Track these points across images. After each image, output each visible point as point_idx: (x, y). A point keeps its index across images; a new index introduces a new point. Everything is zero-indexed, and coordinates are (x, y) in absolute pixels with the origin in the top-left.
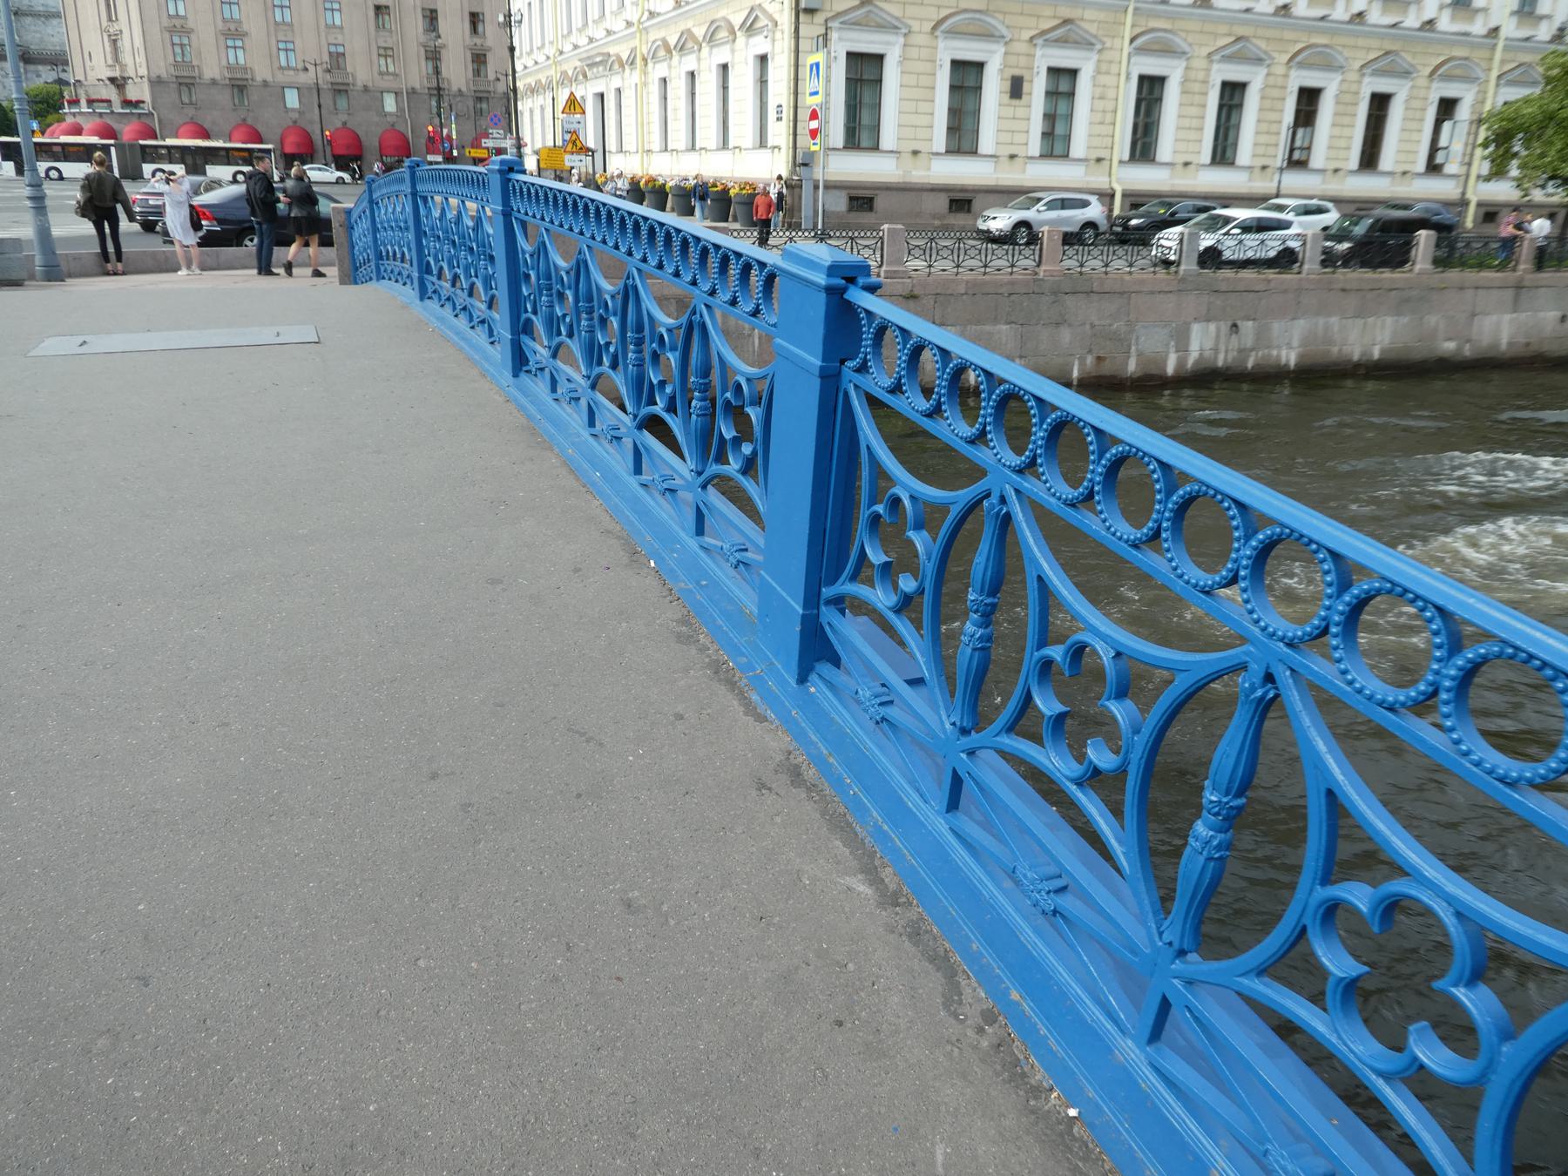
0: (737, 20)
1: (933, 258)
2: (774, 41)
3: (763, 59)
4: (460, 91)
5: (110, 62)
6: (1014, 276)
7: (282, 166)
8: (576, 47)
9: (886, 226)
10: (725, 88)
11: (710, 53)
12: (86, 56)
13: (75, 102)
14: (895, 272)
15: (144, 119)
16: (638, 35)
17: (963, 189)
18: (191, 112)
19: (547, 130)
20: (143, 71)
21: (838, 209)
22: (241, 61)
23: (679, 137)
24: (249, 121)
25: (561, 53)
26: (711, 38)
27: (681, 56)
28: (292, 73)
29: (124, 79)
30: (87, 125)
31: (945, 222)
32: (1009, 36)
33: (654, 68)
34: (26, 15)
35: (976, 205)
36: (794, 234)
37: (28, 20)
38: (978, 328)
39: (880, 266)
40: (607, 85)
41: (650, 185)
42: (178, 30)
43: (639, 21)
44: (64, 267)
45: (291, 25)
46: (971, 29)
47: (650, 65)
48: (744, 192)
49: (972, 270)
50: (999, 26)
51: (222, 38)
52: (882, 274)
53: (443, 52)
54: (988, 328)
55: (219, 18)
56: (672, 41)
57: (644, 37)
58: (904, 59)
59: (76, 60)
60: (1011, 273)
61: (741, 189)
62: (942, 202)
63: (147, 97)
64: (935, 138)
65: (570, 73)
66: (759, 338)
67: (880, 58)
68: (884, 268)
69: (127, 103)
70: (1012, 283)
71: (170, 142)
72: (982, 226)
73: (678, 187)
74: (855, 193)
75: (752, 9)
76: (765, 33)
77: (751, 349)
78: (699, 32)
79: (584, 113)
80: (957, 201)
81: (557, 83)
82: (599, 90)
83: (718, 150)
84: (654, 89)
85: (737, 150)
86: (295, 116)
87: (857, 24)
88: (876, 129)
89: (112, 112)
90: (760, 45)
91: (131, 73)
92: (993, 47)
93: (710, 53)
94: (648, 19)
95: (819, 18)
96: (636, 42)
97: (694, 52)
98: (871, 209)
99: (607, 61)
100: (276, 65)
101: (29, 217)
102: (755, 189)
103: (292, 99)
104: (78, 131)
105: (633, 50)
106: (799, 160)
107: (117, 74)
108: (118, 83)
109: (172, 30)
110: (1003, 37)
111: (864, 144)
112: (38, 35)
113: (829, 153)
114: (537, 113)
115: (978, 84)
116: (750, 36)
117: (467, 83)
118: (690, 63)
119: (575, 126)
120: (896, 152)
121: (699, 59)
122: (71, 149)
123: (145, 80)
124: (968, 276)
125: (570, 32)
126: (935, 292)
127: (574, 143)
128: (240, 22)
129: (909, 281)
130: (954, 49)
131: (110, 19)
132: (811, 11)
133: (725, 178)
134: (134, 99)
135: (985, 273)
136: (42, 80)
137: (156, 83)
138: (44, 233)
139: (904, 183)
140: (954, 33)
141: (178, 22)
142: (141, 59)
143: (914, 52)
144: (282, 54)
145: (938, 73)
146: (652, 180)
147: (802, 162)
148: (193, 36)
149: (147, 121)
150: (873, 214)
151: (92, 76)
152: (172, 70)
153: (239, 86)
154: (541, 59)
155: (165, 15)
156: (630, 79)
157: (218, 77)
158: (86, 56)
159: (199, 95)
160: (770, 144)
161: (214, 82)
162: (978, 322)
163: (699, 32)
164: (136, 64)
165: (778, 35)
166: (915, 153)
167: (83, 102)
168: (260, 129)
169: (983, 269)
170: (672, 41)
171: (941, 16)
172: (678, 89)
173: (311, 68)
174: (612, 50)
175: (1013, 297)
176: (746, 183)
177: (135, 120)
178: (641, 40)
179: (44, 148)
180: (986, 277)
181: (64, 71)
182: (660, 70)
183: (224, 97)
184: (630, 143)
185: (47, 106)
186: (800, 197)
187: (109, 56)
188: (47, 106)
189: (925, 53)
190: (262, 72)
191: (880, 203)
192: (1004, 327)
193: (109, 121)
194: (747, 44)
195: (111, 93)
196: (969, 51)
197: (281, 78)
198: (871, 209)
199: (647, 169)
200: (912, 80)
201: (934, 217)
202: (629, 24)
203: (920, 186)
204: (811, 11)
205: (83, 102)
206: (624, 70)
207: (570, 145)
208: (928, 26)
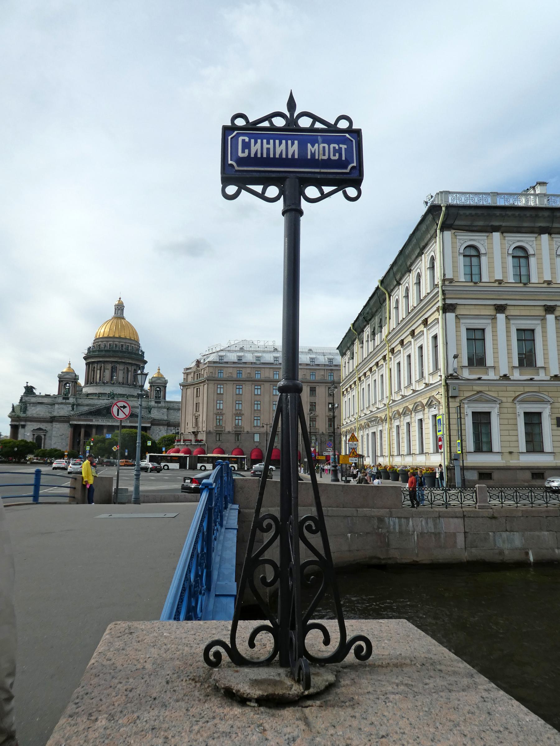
0: (425, 402)
1: (518, 500)
2: (439, 409)
3: (421, 421)
4: (323, 433)
5: (194, 426)
6: (549, 508)
7: (249, 464)
8: (366, 414)
9: (477, 486)
10: (421, 428)
11: (415, 415)
12: (186, 424)
13: (179, 441)
14: (483, 506)
15: (202, 447)
16: (388, 409)
17: (538, 468)
18: (219, 444)
19: (364, 446)
20: (204, 429)
21: (474, 479)
22: (240, 424)
23: (416, 448)
24: (240, 447)
25: (360, 417)
26: (415, 410)
27: (404, 417)
28: (258, 428)
29: (198, 432)
30: (181, 449)
31: (530, 484)
32: (552, 401)
33: (394, 422)
34: (171, 409)
35: (546, 475)
36: (432, 489)
37: (172, 411)
38: (531, 533)
39: (476, 504)
40: (377, 429)
41: (391, 470)
42: (219, 414)
43: (388, 404)
44: (142, 499)
45: (260, 410)
46: (532, 399)
47: (393, 421)
48: (428, 472)
49: (525, 505)
50: (546, 397)
51: (234, 416)
52: (477, 507)
53: (317, 418)
54: (537, 533)
55: (234, 409)
56: (401, 411)
57: (390, 410)
58: (500, 414)
59: (183, 425)
60: (547, 507)
61: (427, 471)
62: (528, 475)
63: (204, 439)
64: (520, 446)
65: (363, 425)
66: (417, 536)
67: (489, 413)
68: (478, 504)
69: (197, 441)
70: (547, 511)
71: (209, 455)
72: (547, 485)
73: (402, 470)
74: (481, 471)
75: (430, 398)
76: (434, 407)
77: (413, 541)
78: (411, 407)
79: (358, 441)
80: (535, 474)
81: (358, 428)
82: (373, 431)
83: (419, 454)
84: (395, 430)
85: (427, 454)
86: (257, 444)
87: (476, 401)
88: (490, 443)
89: (191, 444)
90: (434, 411)
91: (200, 430)
92: (545, 406)
93: (415, 415)
94: (392, 403)
95: (458, 400)
96: (387, 412)
97: (409, 415)
98: (491, 478)
99: (376, 419)
100: (253, 426)
101: (133, 482)
102: (433, 471)
103: (257, 438)
104: (178, 451)
105: (386, 415)
106: (453, 458)
107: (195, 430)
108: (195, 434)
109: (217, 414)
110: (549, 401)
111: (485, 449)
112: (174, 416)
113: (467, 454)
114: (365, 437)
115: (540, 422)
116: (430, 408)
117: (326, 430)
118: (408, 419)
119: (354, 446)
120: (501, 453)
121: (411, 418)
122: (174, 458)
123: (205, 432)
124: (524, 508)
125: (364, 409)
126: (506, 516)
127: (353, 453)
128: (241, 410)
129: (491, 510)
130: (525, 408)
131: (196, 411)
132: (454, 397)
133: (421, 466)
134: (200, 439)
135: (532, 507)
136: (172, 432)
137: (208, 433)
138: (137, 487)
139: (506, 466)
140: (523, 401)
141: (219, 411)
142: (205, 425)
143: (505, 410)
144: (255, 421)
145: (518, 418)
146: (392, 467)
147: (454, 458)
148: (224, 416)
149: (202, 447)
150: (492, 481)
151: (187, 431)
152: (215, 429)
153: (238, 434)
154: (353, 420)
155: (216, 409)
156: (386, 426)
157: (231, 430)
158: (186, 424)
159: (223, 437)
160: (425, 452)
161: (229, 432)
162: (531, 530)
163: (411, 407)
164: (203, 427)
165: (441, 407)
166: (511, 453)
167: (182, 441)
168: (244, 449)
169: (531, 505)
170: (401, 411)
171: (516, 395)
172: (404, 429)
173: (265, 426)
174: (379, 415)
175: (549, 518)
176: (429, 468)
177: (199, 447)
178: (389, 411)
179: (165, 458)
180: (533, 508)
181: (178, 429)
182: (396, 423)
183: (232, 438)
184: (386, 452)
185: (169, 442)
186: (454, 474)
187: (194, 424)
188: (169, 442)
189: (510, 410)
190: (247, 428)
191: (495, 475)
192: (546, 533)
193: (190, 448)
194: (429, 411)
195: (192, 437)
196: (533, 408)
197: (254, 430)
198: (491, 478)
199: (392, 463)
200: (506, 422)
201: (524, 481)
202: (385, 405)
203: (543, 467)
204: (454, 397)
205: (182, 441)
206: (383, 423)
207: (352, 454)
208: (510, 400)
